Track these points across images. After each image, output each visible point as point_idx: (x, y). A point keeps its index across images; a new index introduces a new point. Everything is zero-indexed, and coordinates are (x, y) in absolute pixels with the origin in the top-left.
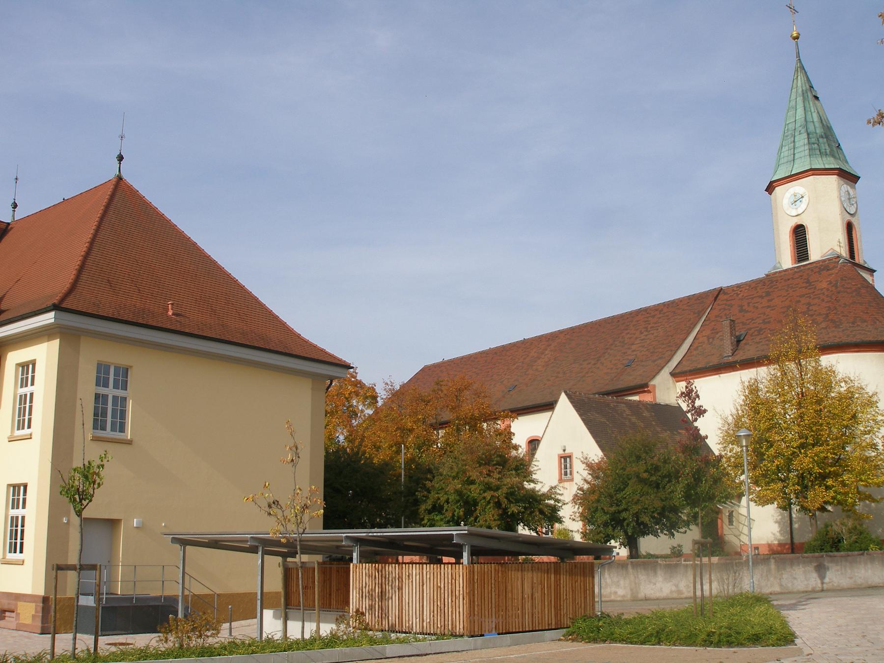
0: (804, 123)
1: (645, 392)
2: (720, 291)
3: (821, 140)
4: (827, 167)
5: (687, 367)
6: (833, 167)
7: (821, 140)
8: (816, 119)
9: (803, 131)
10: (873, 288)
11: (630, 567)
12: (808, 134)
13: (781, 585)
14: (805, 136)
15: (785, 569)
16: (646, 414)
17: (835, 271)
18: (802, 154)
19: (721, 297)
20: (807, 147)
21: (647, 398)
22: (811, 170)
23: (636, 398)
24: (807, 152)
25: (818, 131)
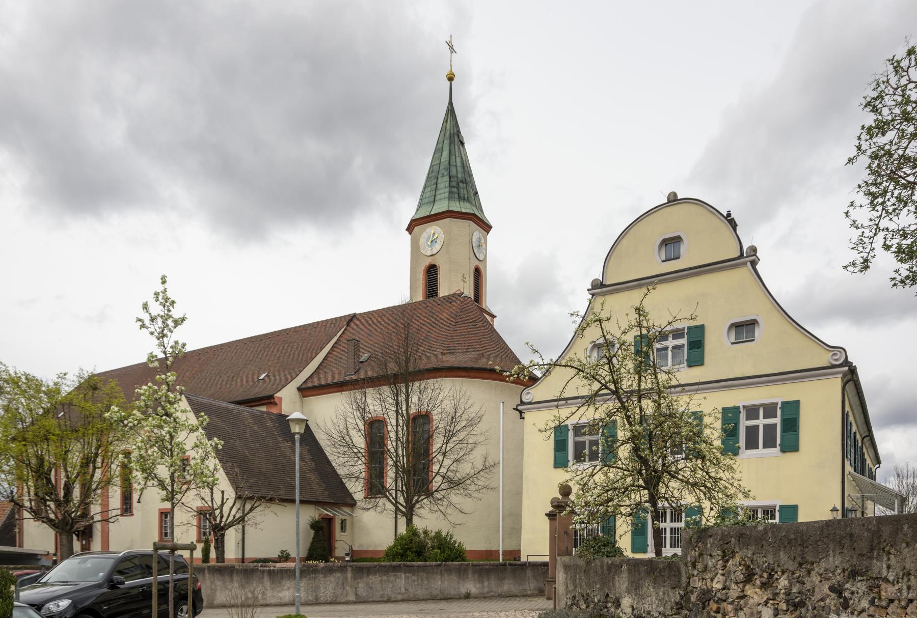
0: (447, 165)
1: (271, 403)
2: (353, 317)
3: (461, 185)
4: (463, 210)
5: (315, 382)
6: (468, 211)
7: (461, 185)
8: (459, 164)
9: (446, 173)
10: (492, 326)
11: (206, 572)
12: (450, 177)
13: (356, 594)
14: (446, 178)
15: (361, 578)
16: (269, 424)
17: (457, 303)
18: (443, 196)
19: (354, 322)
20: (447, 190)
21: (274, 410)
22: (448, 211)
23: (264, 409)
24: (447, 194)
25: (459, 176)
